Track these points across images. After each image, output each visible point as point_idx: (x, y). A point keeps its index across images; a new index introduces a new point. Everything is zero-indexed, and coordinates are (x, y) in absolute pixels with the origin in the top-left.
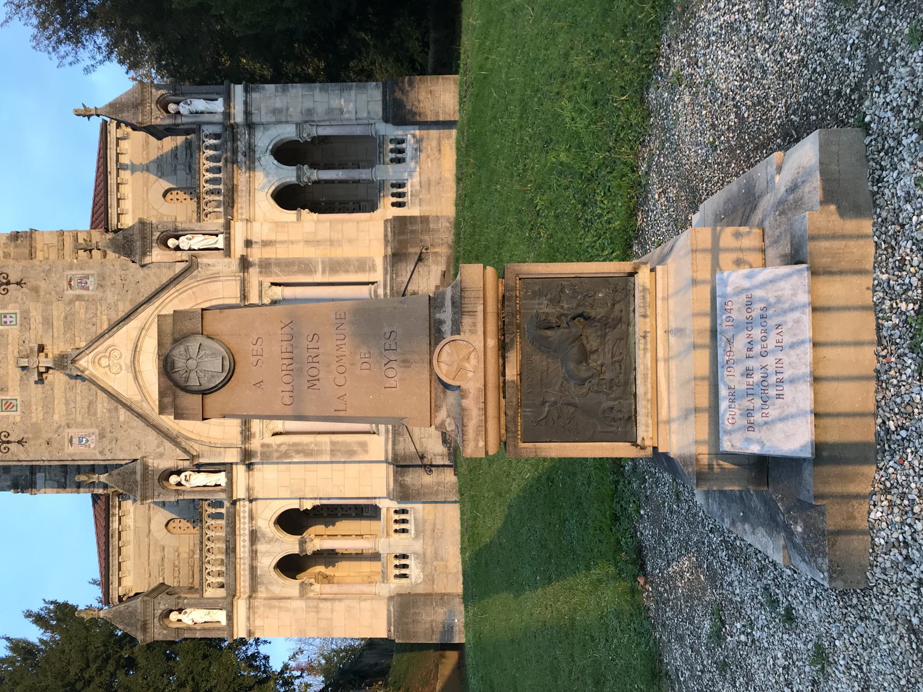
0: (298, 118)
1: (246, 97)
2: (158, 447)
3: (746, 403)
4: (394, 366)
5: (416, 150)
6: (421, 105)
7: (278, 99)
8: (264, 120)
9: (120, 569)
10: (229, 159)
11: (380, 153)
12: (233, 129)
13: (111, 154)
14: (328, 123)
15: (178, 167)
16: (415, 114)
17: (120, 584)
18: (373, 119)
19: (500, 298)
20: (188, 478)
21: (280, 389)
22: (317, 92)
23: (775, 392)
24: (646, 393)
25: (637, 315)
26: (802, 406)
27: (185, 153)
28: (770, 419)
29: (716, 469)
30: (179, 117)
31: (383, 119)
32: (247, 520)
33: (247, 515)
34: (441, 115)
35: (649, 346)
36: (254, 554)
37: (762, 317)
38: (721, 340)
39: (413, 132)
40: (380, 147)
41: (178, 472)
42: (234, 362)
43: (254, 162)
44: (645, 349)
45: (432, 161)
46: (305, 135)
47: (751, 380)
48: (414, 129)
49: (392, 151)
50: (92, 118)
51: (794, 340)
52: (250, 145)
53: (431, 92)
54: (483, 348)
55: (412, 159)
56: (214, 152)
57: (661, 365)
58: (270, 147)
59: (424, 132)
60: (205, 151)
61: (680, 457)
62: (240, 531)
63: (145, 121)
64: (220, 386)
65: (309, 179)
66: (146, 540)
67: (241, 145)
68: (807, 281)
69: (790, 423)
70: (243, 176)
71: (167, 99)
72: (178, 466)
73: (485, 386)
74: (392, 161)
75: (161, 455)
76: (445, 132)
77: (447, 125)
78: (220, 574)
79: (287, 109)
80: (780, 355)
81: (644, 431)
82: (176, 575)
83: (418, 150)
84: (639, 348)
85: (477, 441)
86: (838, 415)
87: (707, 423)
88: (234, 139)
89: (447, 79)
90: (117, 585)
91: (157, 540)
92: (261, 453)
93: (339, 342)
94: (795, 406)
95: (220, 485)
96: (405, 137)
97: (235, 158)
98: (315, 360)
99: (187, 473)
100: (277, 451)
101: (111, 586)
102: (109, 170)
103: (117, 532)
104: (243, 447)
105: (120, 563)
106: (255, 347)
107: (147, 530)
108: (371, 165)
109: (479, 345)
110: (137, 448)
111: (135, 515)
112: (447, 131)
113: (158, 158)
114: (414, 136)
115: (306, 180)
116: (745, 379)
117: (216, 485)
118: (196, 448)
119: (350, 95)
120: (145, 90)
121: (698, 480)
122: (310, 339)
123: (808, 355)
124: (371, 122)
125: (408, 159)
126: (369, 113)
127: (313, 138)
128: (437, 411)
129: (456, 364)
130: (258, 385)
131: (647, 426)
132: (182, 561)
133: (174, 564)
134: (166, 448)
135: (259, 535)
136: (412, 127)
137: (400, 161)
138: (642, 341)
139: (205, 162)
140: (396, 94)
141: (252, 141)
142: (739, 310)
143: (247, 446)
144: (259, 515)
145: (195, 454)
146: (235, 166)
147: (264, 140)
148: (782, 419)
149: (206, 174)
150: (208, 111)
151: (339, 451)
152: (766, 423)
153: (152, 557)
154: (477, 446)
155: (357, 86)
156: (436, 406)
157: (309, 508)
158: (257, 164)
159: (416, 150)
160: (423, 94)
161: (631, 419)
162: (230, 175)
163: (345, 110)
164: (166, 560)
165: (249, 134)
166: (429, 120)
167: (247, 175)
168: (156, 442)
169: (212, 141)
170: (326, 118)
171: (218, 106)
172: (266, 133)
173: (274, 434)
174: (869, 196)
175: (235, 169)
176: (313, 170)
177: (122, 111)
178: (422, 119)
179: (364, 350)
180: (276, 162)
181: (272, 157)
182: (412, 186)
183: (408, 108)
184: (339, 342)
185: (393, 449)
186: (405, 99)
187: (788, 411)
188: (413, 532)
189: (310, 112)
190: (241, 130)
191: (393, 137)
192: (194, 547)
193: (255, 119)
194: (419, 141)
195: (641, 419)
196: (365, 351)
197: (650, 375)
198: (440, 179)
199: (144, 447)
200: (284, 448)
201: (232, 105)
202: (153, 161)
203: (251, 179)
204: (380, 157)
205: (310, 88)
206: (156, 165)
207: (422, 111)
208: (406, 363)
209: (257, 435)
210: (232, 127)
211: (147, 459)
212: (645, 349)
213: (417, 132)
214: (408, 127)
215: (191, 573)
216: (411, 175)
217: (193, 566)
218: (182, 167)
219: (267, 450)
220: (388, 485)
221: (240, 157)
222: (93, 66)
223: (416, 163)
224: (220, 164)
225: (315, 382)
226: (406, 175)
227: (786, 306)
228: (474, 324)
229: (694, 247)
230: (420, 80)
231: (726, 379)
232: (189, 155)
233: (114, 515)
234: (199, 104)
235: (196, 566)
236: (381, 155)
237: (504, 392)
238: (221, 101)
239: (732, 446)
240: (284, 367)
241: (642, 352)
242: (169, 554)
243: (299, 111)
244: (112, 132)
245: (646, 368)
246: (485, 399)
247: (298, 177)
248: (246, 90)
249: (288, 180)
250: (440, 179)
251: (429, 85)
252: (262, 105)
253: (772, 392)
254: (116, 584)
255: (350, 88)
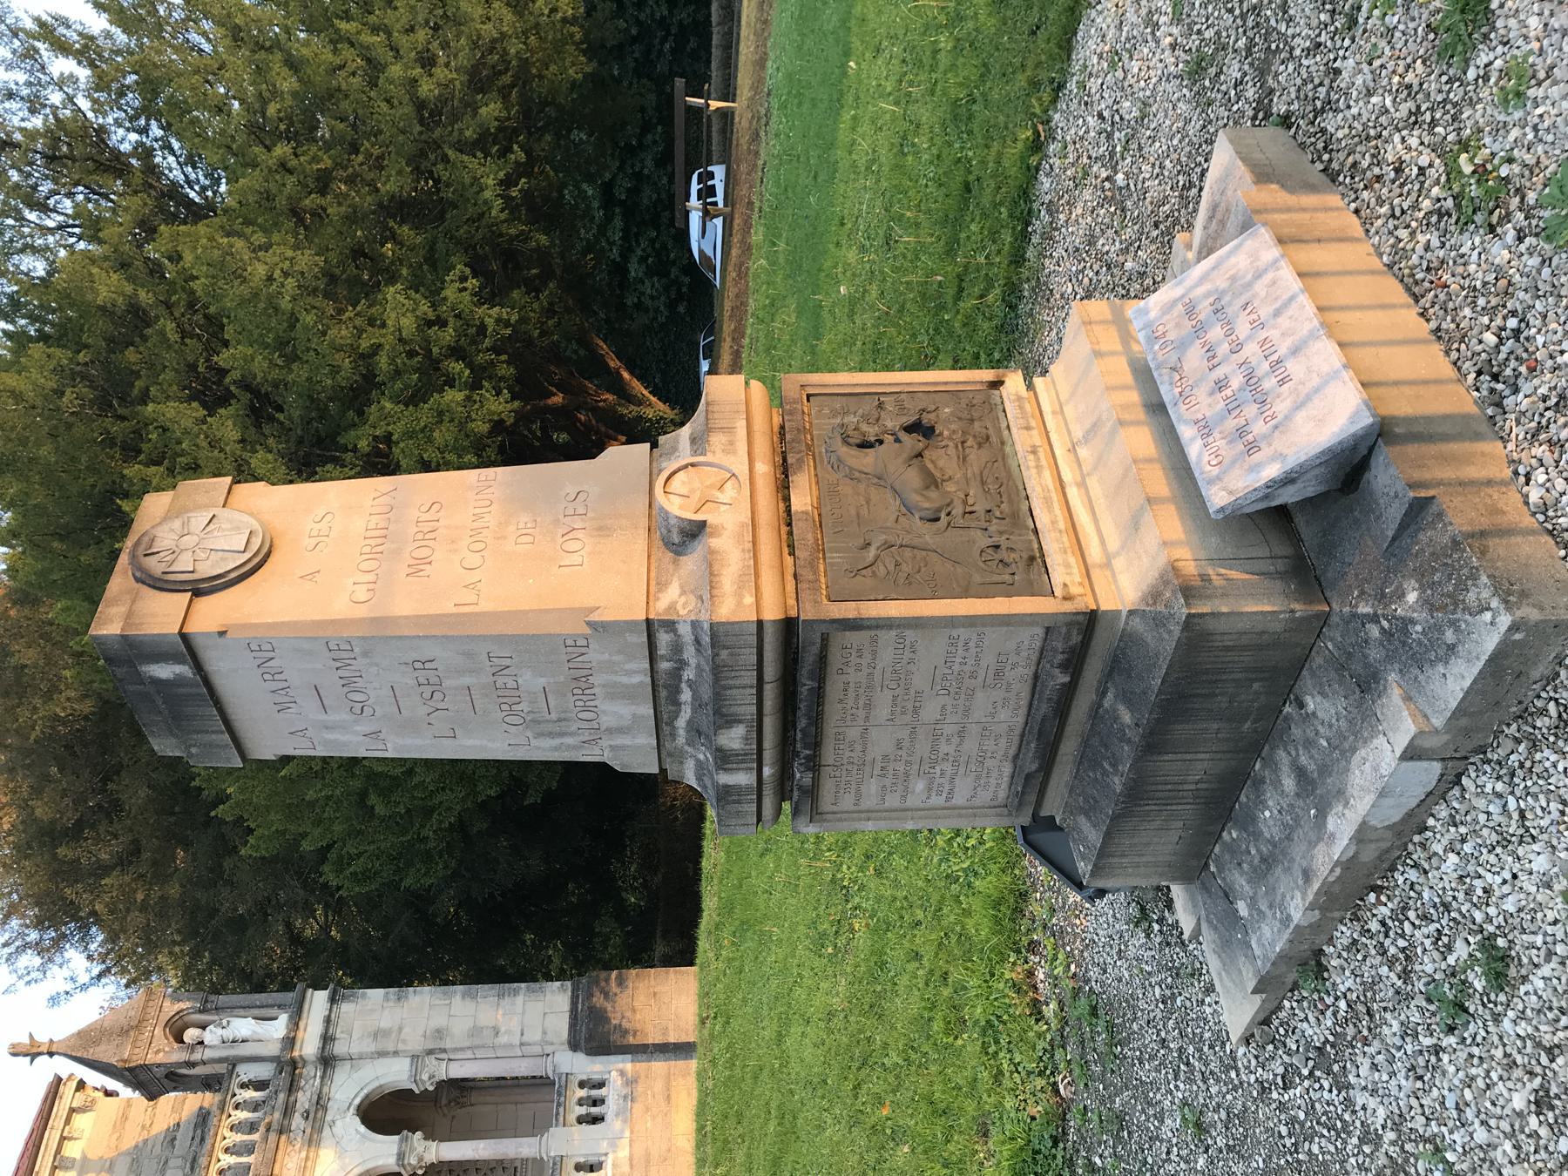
0: (415, 1043)
1: (331, 1010)
3: (1232, 423)
5: (625, 1097)
6: (638, 1016)
7: (386, 1012)
8: (355, 1050)
10: (275, 1126)
11: (559, 1105)
12: (295, 1069)
13: (57, 1122)
14: (469, 1054)
15: (172, 1163)
16: (626, 1032)
18: (552, 1044)
19: (776, 429)
22: (458, 998)
23: (1274, 381)
24: (1054, 522)
25: (1014, 430)
26: (1326, 369)
27: (191, 1135)
28: (1280, 417)
29: (1217, 582)
30: (199, 1049)
31: (569, 1043)
34: (672, 1033)
35: (1044, 462)
37: (1216, 312)
38: (1160, 375)
39: (621, 1066)
40: (559, 1094)
42: (268, 555)
43: (321, 1130)
44: (1038, 467)
45: (654, 1118)
46: (425, 1077)
47: (1229, 392)
48: (623, 1061)
49: (580, 1103)
50: (39, 1060)
51: (1277, 305)
52: (319, 1098)
53: (655, 994)
55: (617, 1115)
56: (250, 1115)
57: (1073, 493)
58: (357, 1101)
59: (642, 1066)
60: (233, 1113)
61: (1144, 599)
63: (134, 1058)
64: (233, 575)
65: (421, 1159)
67: (303, 1099)
68: (1267, 236)
69: (1316, 401)
70: (295, 1159)
71: (186, 1019)
73: (753, 519)
74: (580, 1120)
76: (678, 1065)
77: (682, 1050)
79: (400, 1029)
80: (1263, 334)
81: (1063, 571)
83: (630, 1098)
84: (1028, 468)
85: (739, 596)
86: (1396, 383)
87: (1176, 518)
88: (292, 1088)
89: (682, 973)
93: (478, 511)
94: (1315, 375)
96: (606, 1076)
97: (286, 1122)
102: (36, 1169)
108: (537, 1128)
109: (742, 468)
112: (681, 1063)
113: (136, 1146)
114: (622, 1073)
115: (413, 1161)
116: (1219, 396)
119: (513, 1004)
120: (151, 1004)
121: (1186, 597)
123: (1308, 307)
124: (548, 1049)
125: (608, 1118)
126: (544, 1033)
127: (441, 1085)
128: (660, 591)
129: (698, 492)
131: (1068, 566)
136: (621, 1057)
137: (596, 1120)
138: (1031, 457)
139: (227, 1133)
140: (595, 999)
141: (326, 1089)
142: (1178, 325)
146: (283, 1137)
147: (348, 1088)
148: (1298, 406)
149: (222, 1156)
150: (256, 1037)
152: (1276, 427)
154: (739, 603)
155: (528, 989)
156: (658, 584)
158: (326, 1131)
159: (625, 1097)
160: (642, 998)
161: (1036, 560)
162: (270, 1155)
163: (503, 1029)
165: (323, 1078)
166: (651, 1041)
167: (304, 1154)
169: (250, 1094)
170: (467, 1044)
171: (278, 1028)
172: (355, 1076)
174: (1322, 176)
175: (281, 1145)
176: (430, 1143)
177: (96, 1042)
178: (639, 1040)
179: (524, 518)
180: (363, 1129)
181: (358, 1120)
182: (615, 1166)
183: (614, 1022)
184: (478, 511)
186: (609, 1008)
187: (1304, 390)
189: (439, 1033)
190: (309, 1071)
191: (584, 1077)
193: (339, 1048)
194: (631, 1082)
195: (1054, 559)
196: (526, 520)
197: (1055, 499)
198: (669, 1150)
201: (302, 1024)
202: (128, 1153)
203: (309, 1164)
204: (558, 1114)
205: (445, 994)
206: (129, 1159)
207: (638, 1027)
208: (602, 531)
210: (293, 1064)
212: (1038, 467)
213: (629, 1067)
214: (612, 1058)
216: (613, 1145)
218: (179, 1162)
221: (297, 1121)
222: (67, 993)
223: (625, 1121)
224: (256, 1137)
226: (604, 1146)
227: (1249, 277)
228: (731, 443)
229: (1087, 319)
230: (637, 975)
231: (1187, 416)
232: (197, 1140)
234: (243, 1026)
236: (561, 1110)
237: (791, 547)
238: (283, 1018)
239: (1231, 493)
240: (367, 549)
241: (1034, 471)
243: (422, 1032)
244: (64, 1097)
245: (1045, 489)
246: (754, 536)
247: (401, 1156)
248: (333, 1000)
249: (380, 1163)
250: (669, 1150)
251: (653, 983)
252: (357, 1024)
253: (1269, 383)
255: (516, 992)
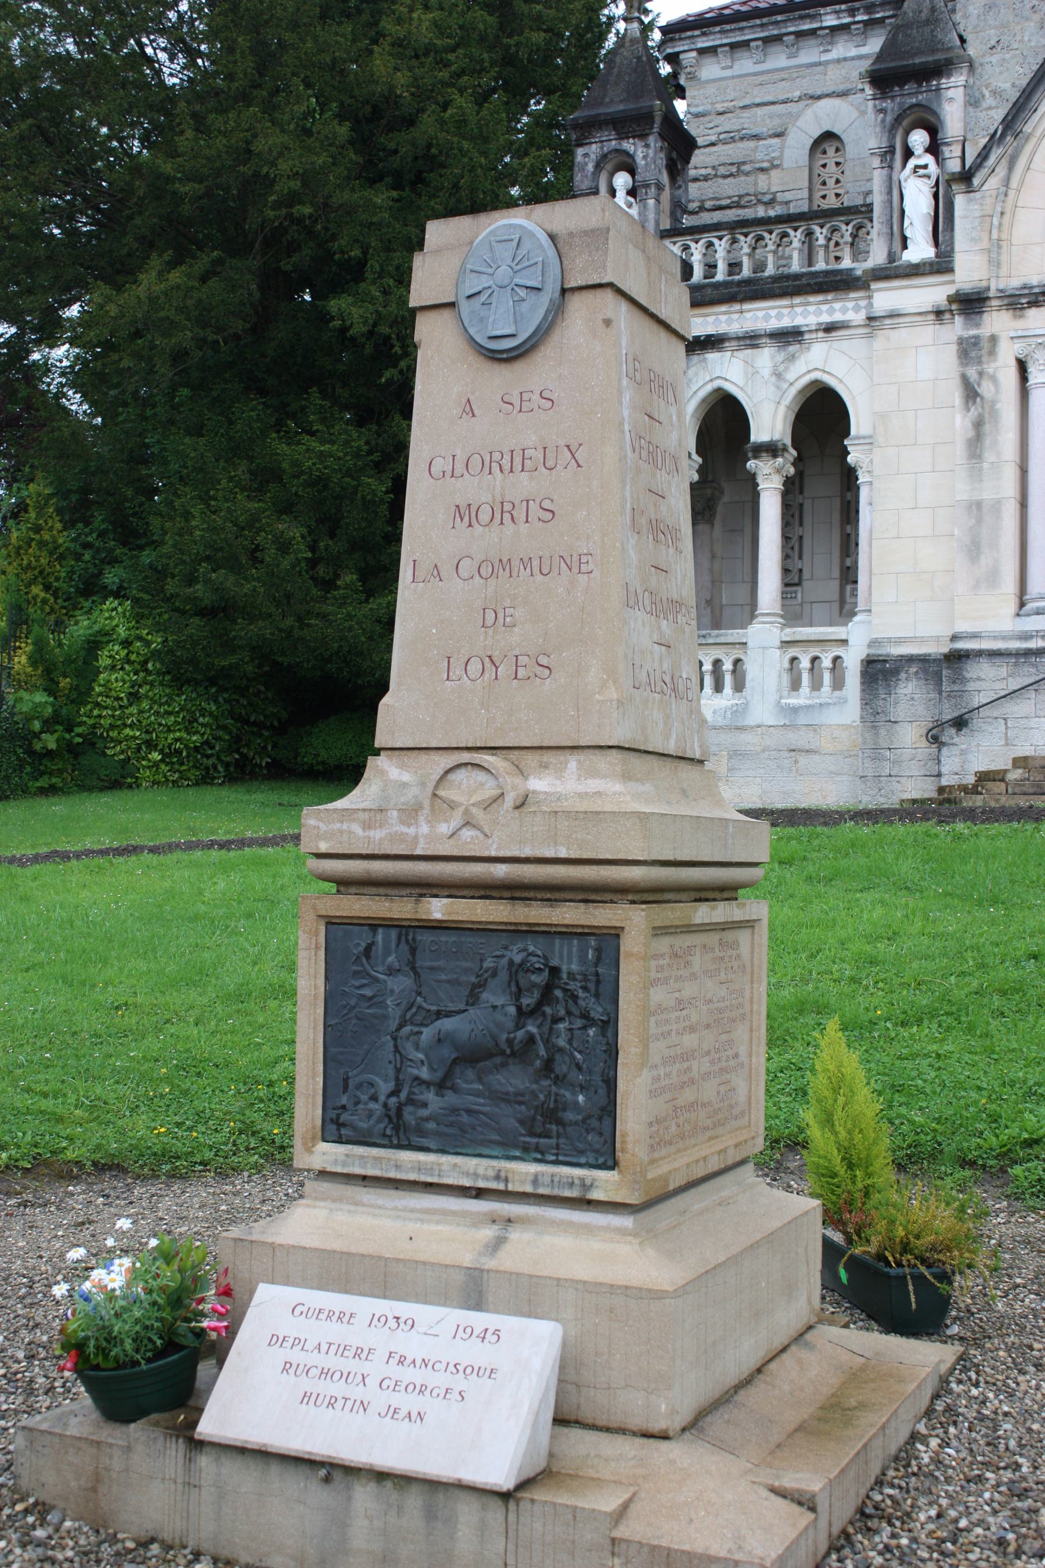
2: (994, 93)
4: (487, 675)
9: (734, 46)
17: (702, 52)
20: (922, 172)
21: (458, 452)
32: (826, 318)
33: (838, 317)
36: (751, 340)
41: (934, 149)
54: (486, 854)
62: (725, 313)
66: (797, 94)
72: (947, 144)
75: (973, 102)
78: (711, 267)
82: (722, 170)
90: (700, 45)
91: (798, 116)
92: (977, 338)
93: (536, 563)
95: (905, 247)
98: (507, 516)
99: (933, 169)
100: (981, 374)
101: (697, 33)
103: (815, 25)
104: (991, 294)
105: (745, 44)
106: (536, 397)
107: (819, 93)
110: (993, 43)
111: (853, 59)
117: (904, 240)
118: (989, 183)
122: (547, 504)
130: (468, 409)
132: (750, 179)
133: (744, 163)
134: (992, 113)
135: (791, 349)
138: (491, 1173)
143: (995, 303)
144: (836, 344)
145: (976, 181)
151: (979, 521)
153: (759, 112)
157: (849, 459)
164: (752, 144)
168: (1008, 85)
173: (1022, 366)
184: (536, 563)
185: (980, 653)
188: (793, 701)
192: (781, 203)
199: (994, 59)
200: (986, 389)
209: (1020, 324)
211: (965, 71)
215: (724, 202)
217: (738, 206)
219: (984, 352)
220: (900, 641)
225: (466, 519)
233: (852, 12)
235: (740, 212)
242: (762, 151)
254: (703, 43)
